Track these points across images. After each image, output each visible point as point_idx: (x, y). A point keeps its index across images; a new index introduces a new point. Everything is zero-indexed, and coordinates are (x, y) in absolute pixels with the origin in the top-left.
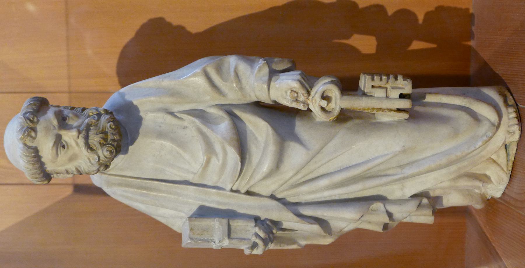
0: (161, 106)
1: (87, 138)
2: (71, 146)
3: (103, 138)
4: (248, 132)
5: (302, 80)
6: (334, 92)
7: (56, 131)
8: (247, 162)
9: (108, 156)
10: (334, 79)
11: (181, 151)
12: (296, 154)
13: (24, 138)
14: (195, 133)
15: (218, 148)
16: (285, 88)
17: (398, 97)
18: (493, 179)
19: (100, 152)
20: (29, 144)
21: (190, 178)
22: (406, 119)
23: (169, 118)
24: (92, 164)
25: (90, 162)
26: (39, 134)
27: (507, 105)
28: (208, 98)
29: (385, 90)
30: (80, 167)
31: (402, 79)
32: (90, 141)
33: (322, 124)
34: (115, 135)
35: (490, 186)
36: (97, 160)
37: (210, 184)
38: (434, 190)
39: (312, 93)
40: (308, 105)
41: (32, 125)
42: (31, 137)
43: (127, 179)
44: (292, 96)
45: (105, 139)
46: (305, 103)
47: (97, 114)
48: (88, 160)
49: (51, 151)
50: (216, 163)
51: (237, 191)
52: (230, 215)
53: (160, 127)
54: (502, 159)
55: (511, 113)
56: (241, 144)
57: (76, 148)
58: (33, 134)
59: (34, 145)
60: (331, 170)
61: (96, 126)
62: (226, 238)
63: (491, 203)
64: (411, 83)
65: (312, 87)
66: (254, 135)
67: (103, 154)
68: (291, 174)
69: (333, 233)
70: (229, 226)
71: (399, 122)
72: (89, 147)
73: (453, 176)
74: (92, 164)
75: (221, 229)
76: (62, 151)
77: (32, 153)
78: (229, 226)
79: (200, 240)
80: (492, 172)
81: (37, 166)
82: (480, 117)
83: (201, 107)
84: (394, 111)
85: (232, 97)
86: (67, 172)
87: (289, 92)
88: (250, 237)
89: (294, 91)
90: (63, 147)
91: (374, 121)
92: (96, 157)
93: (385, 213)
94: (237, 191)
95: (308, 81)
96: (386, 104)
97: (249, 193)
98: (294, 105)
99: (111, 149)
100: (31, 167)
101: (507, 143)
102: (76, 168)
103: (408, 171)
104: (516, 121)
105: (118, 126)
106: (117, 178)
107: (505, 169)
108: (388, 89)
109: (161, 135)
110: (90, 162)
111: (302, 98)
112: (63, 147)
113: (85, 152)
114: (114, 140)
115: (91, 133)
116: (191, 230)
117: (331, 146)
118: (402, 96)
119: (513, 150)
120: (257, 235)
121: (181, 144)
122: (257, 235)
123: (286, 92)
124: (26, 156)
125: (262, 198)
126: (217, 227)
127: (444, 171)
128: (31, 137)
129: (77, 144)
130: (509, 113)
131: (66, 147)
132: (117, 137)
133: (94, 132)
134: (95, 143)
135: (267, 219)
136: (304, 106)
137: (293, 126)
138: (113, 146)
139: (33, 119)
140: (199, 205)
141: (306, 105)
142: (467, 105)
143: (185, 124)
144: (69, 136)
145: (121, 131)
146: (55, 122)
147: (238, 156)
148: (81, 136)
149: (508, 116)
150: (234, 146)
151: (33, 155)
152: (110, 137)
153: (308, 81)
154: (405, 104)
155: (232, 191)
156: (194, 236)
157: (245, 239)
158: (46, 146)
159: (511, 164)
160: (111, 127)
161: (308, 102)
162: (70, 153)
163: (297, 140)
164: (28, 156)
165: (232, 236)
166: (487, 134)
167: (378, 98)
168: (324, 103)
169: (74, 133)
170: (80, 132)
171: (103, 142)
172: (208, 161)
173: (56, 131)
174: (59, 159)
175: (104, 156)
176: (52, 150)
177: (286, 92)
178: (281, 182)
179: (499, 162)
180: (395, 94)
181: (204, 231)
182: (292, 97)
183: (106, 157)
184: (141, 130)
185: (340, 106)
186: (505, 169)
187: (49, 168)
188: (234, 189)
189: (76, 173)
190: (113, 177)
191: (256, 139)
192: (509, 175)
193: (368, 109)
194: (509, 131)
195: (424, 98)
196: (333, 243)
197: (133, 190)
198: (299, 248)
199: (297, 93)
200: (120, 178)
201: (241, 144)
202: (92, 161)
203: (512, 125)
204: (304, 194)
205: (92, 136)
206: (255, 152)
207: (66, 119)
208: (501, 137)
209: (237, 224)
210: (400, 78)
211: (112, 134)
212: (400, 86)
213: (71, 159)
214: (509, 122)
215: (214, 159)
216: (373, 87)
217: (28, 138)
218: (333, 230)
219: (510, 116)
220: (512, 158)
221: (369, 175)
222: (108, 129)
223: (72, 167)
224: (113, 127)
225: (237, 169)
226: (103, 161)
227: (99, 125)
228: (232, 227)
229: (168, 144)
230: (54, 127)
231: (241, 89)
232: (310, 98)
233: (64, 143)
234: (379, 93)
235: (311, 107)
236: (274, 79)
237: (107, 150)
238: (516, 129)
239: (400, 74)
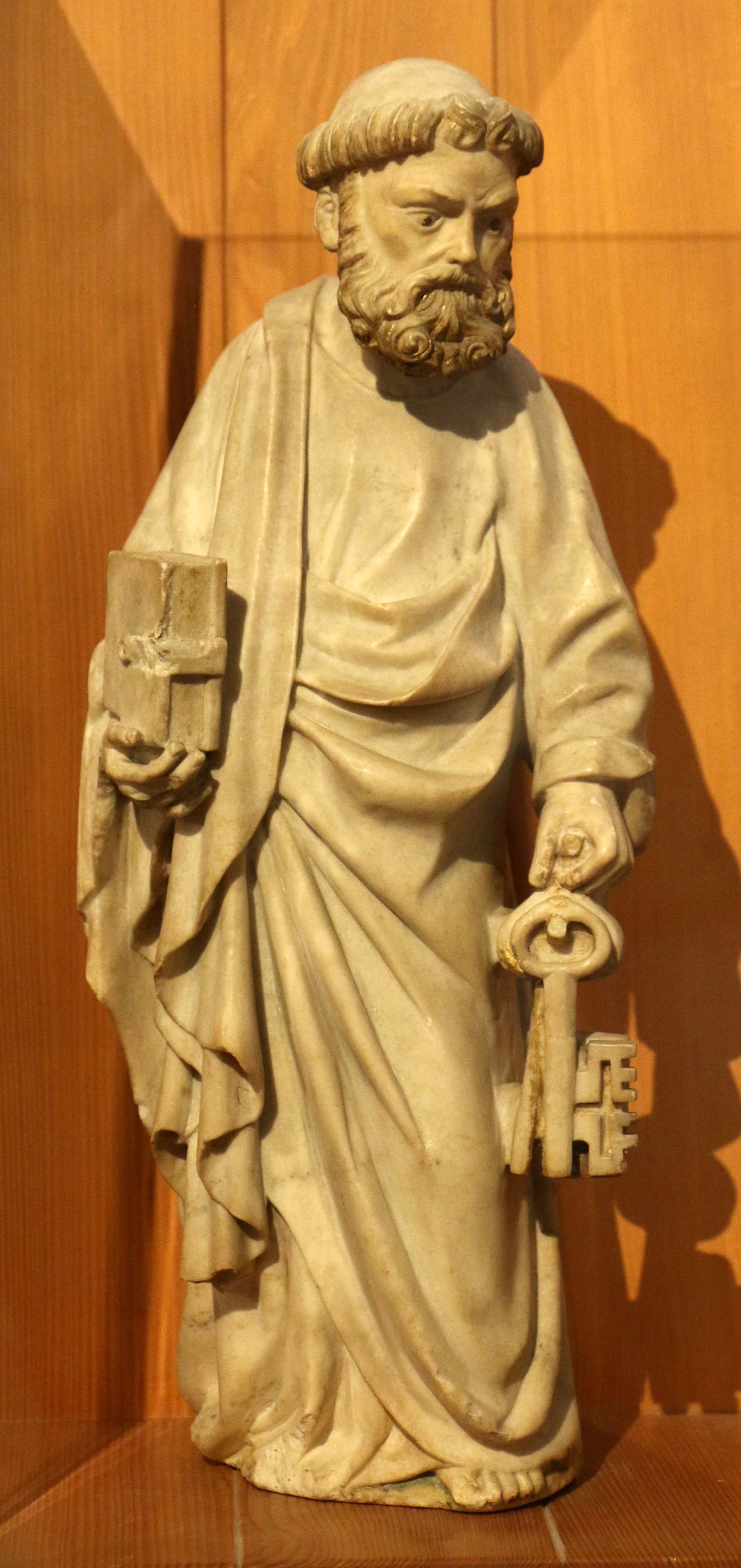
0: (515, 488)
1: (449, 284)
2: (428, 243)
3: (446, 330)
4: (459, 727)
5: (616, 868)
6: (586, 957)
7: (471, 203)
8: (382, 723)
9: (401, 341)
10: (619, 956)
11: (397, 542)
12: (402, 859)
13: (458, 115)
14: (445, 583)
15: (418, 643)
16: (580, 824)
17: (577, 1137)
18: (317, 1451)
19: (411, 320)
20: (442, 132)
21: (319, 568)
22: (508, 1167)
23: (481, 510)
24: (378, 299)
25: (383, 293)
26: (466, 157)
27: (550, 1467)
28: (543, 617)
29: (595, 1097)
30: (366, 266)
31: (627, 1145)
32: (440, 294)
33: (482, 937)
34: (456, 362)
35: (296, 1444)
36: (390, 312)
37: (308, 625)
38: (287, 1277)
39: (578, 897)
40: (543, 888)
41: (491, 137)
42: (462, 136)
43: (303, 396)
44: (570, 842)
45: (443, 336)
46: (548, 879)
47: (501, 312)
48: (387, 286)
49: (420, 186)
50: (375, 637)
51: (293, 701)
52: (230, 684)
53: (458, 486)
54: (385, 1469)
55: (530, 1480)
56: (434, 709)
57: (423, 256)
58: (468, 140)
59: (439, 142)
60: (354, 964)
61: (476, 310)
62: (174, 670)
63: (218, 1468)
64: (619, 1169)
65: (593, 896)
66: (455, 741)
67: (408, 328)
68: (351, 848)
69: (160, 981)
70: (203, 678)
71: (496, 1149)
72: (430, 287)
73: (338, 1320)
74: (378, 299)
75: (199, 655)
76: (415, 218)
77: (418, 135)
78: (203, 678)
79: (168, 597)
80: (343, 1447)
81: (379, 148)
82: (513, 1387)
83: (512, 597)
84: (534, 1131)
85: (545, 685)
86: (346, 231)
87: (581, 834)
88: (174, 736)
89: (582, 847)
90: (428, 222)
91: (494, 1078)
92: (399, 309)
93: (230, 1128)
94: (293, 701)
95: (606, 887)
96: (555, 1102)
97: (289, 730)
98: (542, 849)
99: (421, 349)
100: (378, 132)
101: (446, 1474)
102: (361, 256)
103: (360, 1188)
104: (510, 1492)
105: (470, 366)
106: (304, 369)
107: (357, 1481)
108: (595, 1110)
109: (438, 488)
110: (383, 293)
111: (563, 870)
112: (428, 222)
113: (414, 279)
114: (442, 357)
115: (460, 295)
116: (195, 572)
117: (426, 958)
118: (580, 1148)
119: (422, 1496)
120: (181, 756)
121: (417, 543)
122: (181, 756)
123: (576, 826)
124: (411, 120)
125: (275, 769)
126: (202, 643)
127: (355, 1291)
128: (462, 136)
129: (434, 259)
130: (528, 1473)
131: (428, 228)
132: (448, 366)
133: (464, 305)
134: (435, 307)
135: (215, 785)
136: (542, 875)
137: (472, 855)
138: (429, 356)
139: (506, 141)
140: (246, 597)
141: (544, 881)
142: (538, 1352)
143: (468, 556)
144: (455, 238)
145: (450, 377)
146: (493, 199)
147: (409, 695)
148: (457, 268)
149: (521, 1471)
150: (433, 684)
151: (414, 139)
152: (449, 348)
153: (606, 887)
154: (557, 1160)
155: (296, 684)
156: (176, 578)
157: (169, 722)
158: (421, 176)
159: (373, 1495)
160: (475, 349)
161: (552, 890)
162: (412, 240)
163: (444, 864)
164: (410, 126)
165: (178, 687)
166: (475, 1406)
167: (573, 1082)
168: (558, 929)
169: (466, 252)
170: (467, 266)
171: (438, 328)
172: (378, 616)
173: (471, 203)
174: (394, 210)
175: (403, 332)
176: (423, 191)
177: (576, 826)
178: (323, 823)
179: (378, 1461)
180: (585, 1127)
181: (192, 609)
182: (566, 843)
183: (398, 337)
184: (448, 437)
185: (548, 974)
186: (357, 1481)
187: (363, 184)
188: (301, 692)
189: (347, 254)
190: (304, 359)
191: (443, 748)
192: (336, 1495)
193: (537, 1056)
194: (480, 1476)
195: (547, 1231)
196: (94, 996)
197: (272, 411)
198: (81, 896)
199: (577, 856)
200: (304, 376)
201: (434, 709)
202: (386, 298)
203: (497, 1482)
204: (285, 890)
205: (453, 298)
206: (410, 745)
207: (494, 229)
208: (461, 1450)
209: (208, 698)
210: (631, 1140)
211: (457, 354)
212: (607, 1143)
213: (394, 246)
214: (505, 1473)
215: (389, 632)
216: (605, 1064)
217: (458, 128)
218: (169, 983)
219: (520, 1475)
220: (393, 1497)
221: (343, 1073)
222: (471, 342)
223: (367, 242)
224: (475, 357)
225: (366, 696)
226: (387, 329)
227: (477, 317)
228: (200, 688)
229: (415, 506)
230: (481, 198)
231: (574, 706)
232: (566, 893)
233: (437, 223)
234: (587, 1085)
235: (535, 898)
236: (609, 792)
237: (417, 339)
238: (490, 1493)
239: (640, 1141)
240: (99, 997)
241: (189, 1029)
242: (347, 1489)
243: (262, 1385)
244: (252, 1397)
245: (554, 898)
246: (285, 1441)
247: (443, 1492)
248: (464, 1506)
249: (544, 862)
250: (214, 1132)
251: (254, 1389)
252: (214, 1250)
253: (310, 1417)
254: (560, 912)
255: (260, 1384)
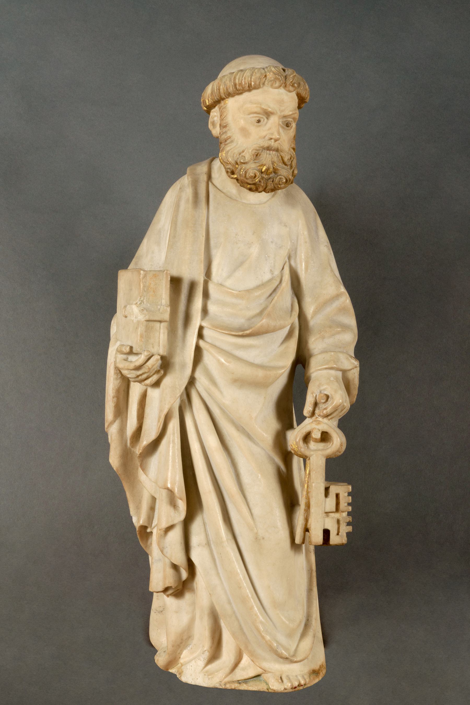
36: (242, 161)
54: (240, 674)
101: (264, 676)
118: (326, 533)
119: (253, 687)
151: (253, 83)
168: (317, 435)
179: (237, 670)
210: (350, 529)
220: (244, 687)
234: (330, 503)
235: (307, 421)
240: (115, 469)
241: (153, 480)
242: (223, 682)
243: (183, 640)
244: (181, 643)
245: (315, 421)
246: (195, 662)
247: (265, 684)
248: (274, 690)
249: (310, 405)
250: (164, 525)
251: (182, 639)
252: (165, 578)
253: (206, 651)
254: (317, 427)
255: (185, 638)
